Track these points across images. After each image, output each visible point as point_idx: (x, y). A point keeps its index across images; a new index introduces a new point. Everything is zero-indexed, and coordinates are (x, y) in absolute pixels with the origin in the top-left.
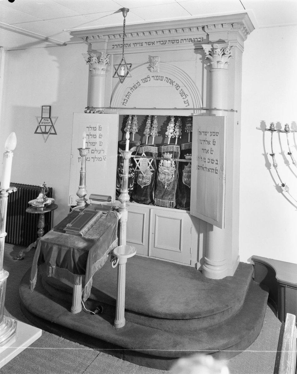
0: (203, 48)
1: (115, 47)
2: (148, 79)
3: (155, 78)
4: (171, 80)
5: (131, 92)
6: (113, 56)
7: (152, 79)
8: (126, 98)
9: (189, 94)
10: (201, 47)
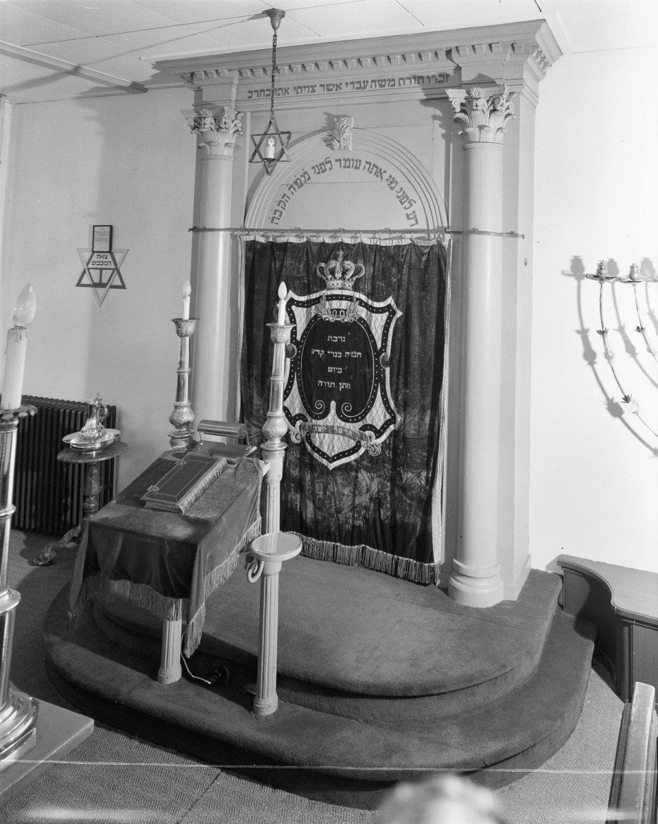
0: (448, 98)
1: (255, 95)
2: (328, 166)
3: (343, 162)
4: (377, 167)
6: (249, 114)
7: (336, 165)
10: (443, 96)
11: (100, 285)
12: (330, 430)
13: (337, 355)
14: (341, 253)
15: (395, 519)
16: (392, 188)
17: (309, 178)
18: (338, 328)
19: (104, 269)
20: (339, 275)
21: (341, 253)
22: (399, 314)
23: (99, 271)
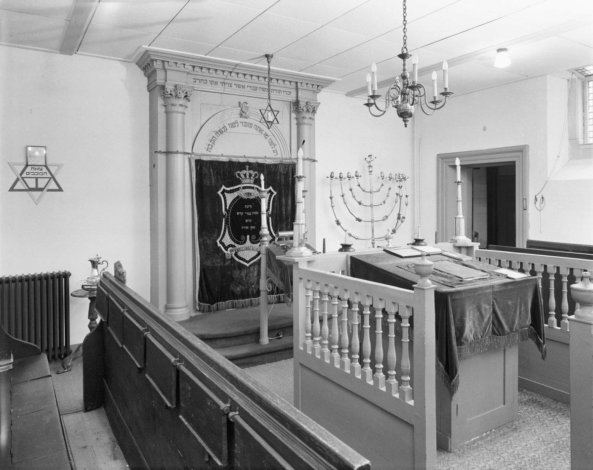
1: (198, 81)
2: (236, 124)
3: (244, 124)
4: (260, 128)
5: (216, 136)
7: (240, 125)
8: (211, 143)
9: (277, 143)
11: (37, 189)
12: (247, 249)
13: (249, 214)
14: (247, 167)
15: (259, 289)
16: (266, 138)
17: (227, 130)
18: (248, 201)
19: (39, 178)
20: (248, 177)
21: (247, 167)
22: (275, 193)
23: (35, 179)
